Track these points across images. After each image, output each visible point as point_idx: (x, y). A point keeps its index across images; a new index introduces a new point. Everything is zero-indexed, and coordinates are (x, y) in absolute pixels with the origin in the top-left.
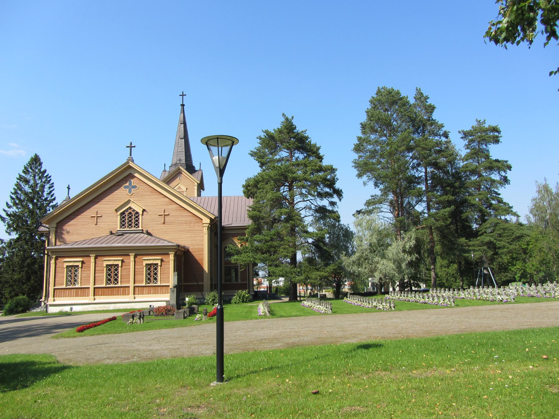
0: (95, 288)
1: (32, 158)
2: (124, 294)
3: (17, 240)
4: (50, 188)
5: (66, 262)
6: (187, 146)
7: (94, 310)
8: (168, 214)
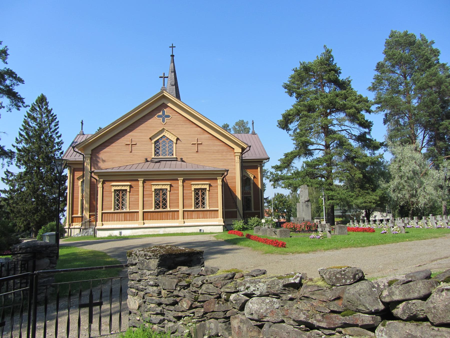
0: (144, 212)
1: (39, 98)
2: (173, 218)
3: (26, 173)
4: (55, 126)
5: (113, 186)
6: (178, 93)
7: (144, 234)
8: (201, 143)
